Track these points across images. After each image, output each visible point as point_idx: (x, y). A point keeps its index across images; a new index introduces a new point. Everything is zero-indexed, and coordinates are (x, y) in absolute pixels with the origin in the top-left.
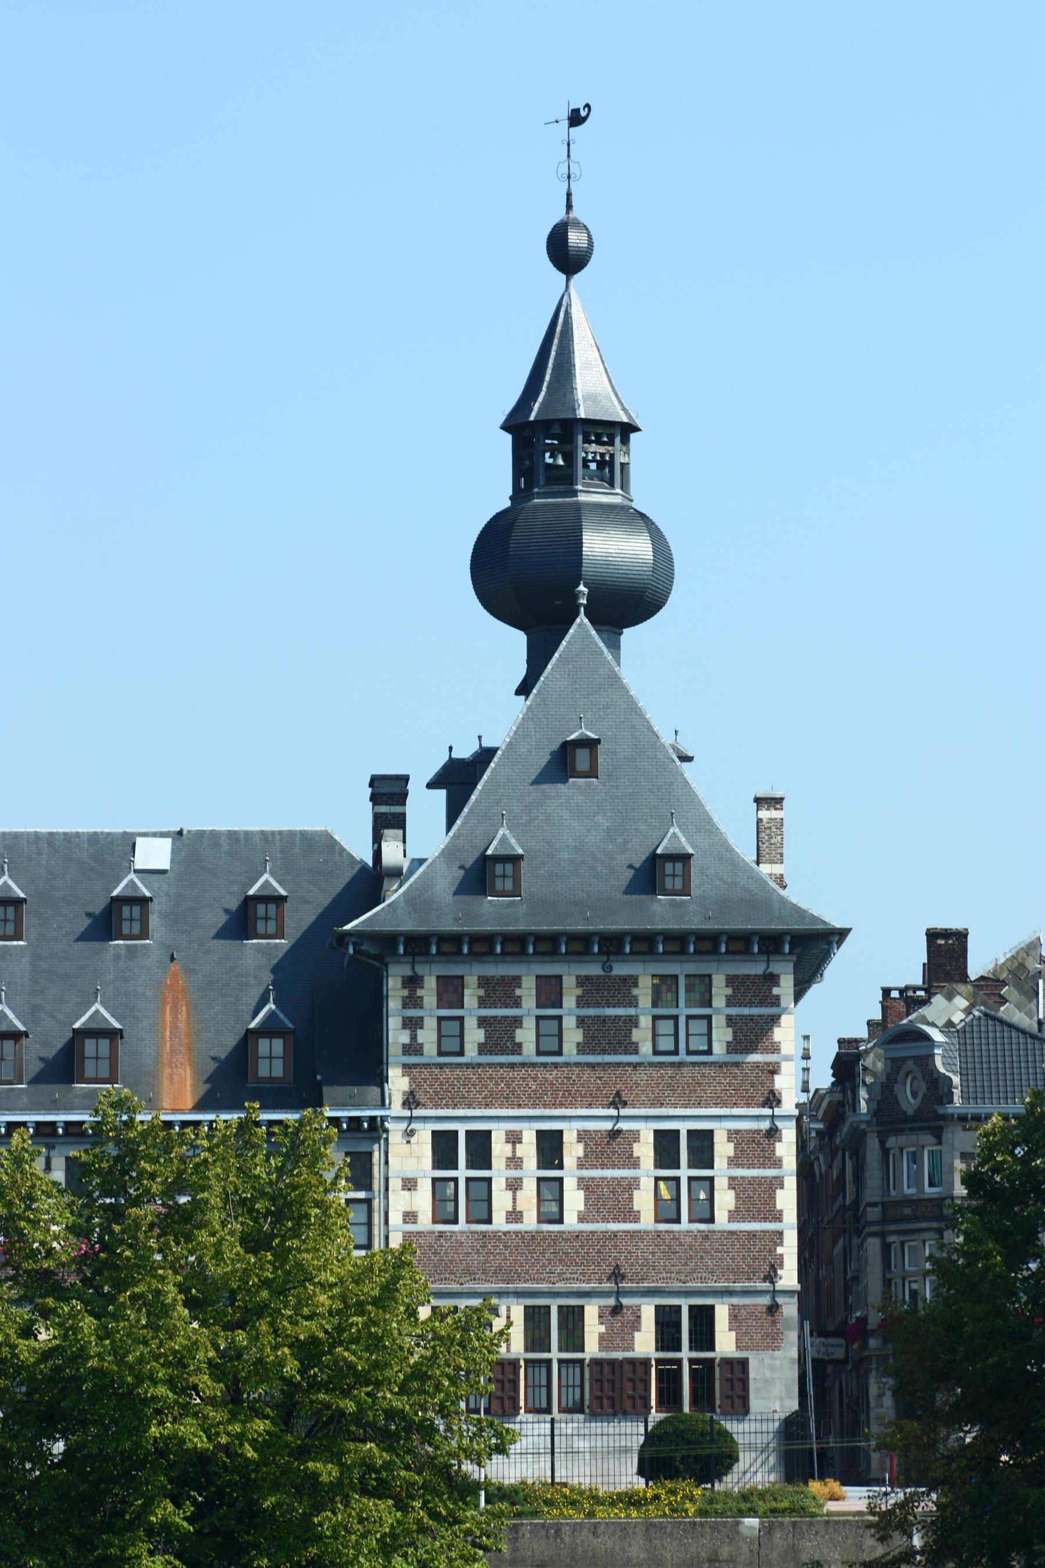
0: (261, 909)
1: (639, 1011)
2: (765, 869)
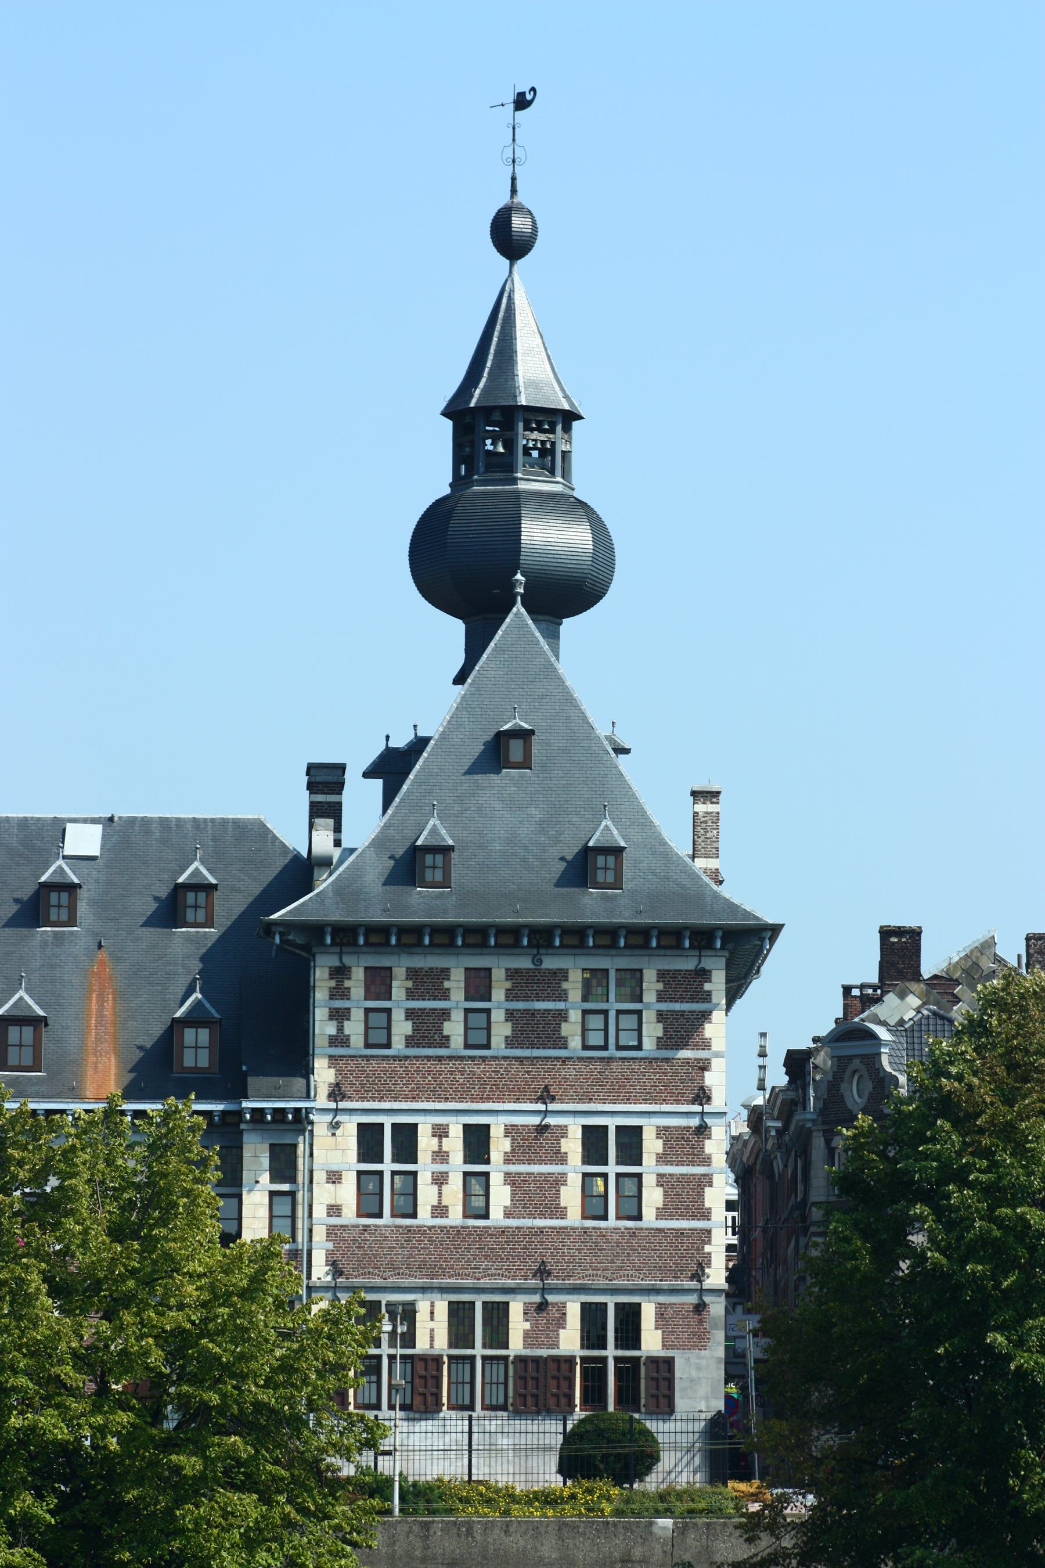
0: (190, 897)
1: (568, 1005)
2: (700, 863)
